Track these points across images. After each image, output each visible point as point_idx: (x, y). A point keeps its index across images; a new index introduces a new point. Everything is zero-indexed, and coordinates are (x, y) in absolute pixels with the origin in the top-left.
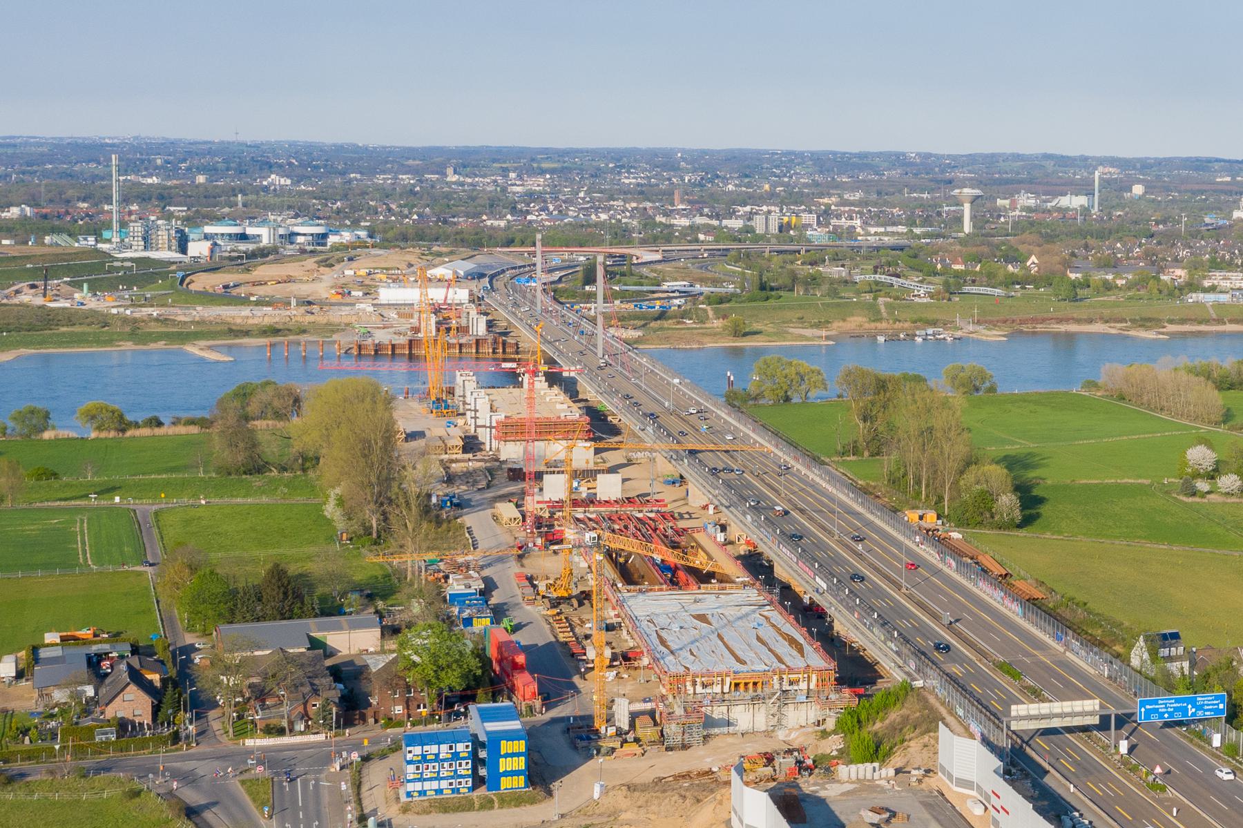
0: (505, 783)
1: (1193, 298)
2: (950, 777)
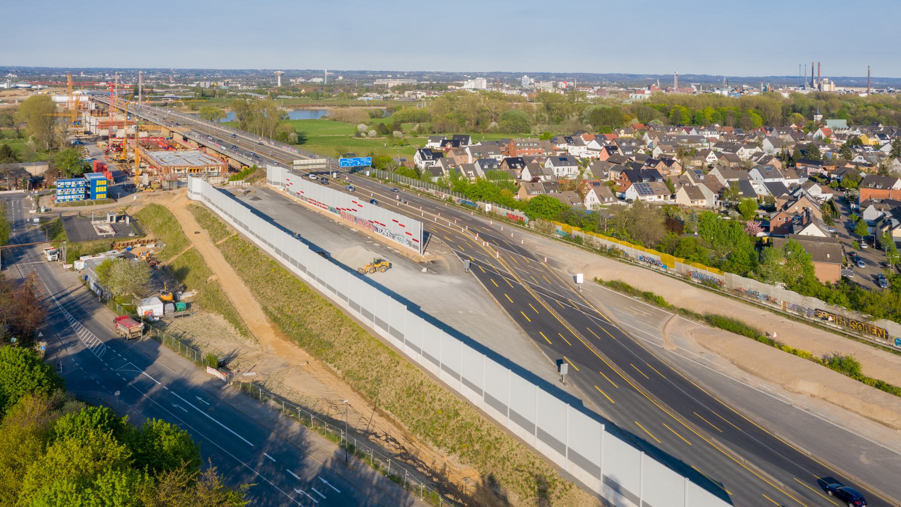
0: (98, 196)
1: (359, 99)
2: (271, 182)
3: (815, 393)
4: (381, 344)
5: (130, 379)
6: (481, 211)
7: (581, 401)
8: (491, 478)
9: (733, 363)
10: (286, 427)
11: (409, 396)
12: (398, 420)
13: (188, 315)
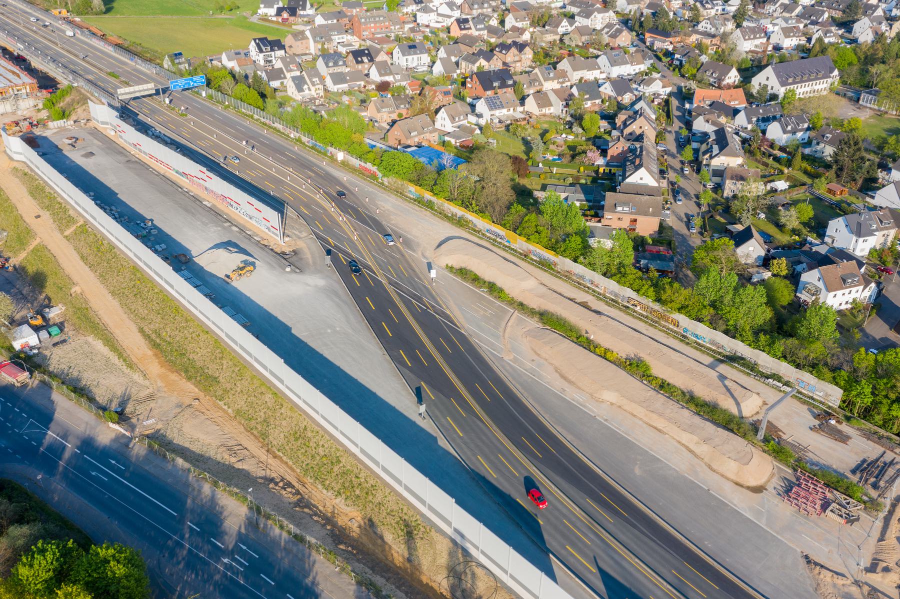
2: (98, 121)
3: (614, 402)
4: (263, 384)
5: (40, 444)
6: (333, 159)
7: (436, 438)
8: (370, 520)
9: (556, 371)
10: (199, 491)
11: (297, 439)
12: (290, 463)
13: (64, 341)
